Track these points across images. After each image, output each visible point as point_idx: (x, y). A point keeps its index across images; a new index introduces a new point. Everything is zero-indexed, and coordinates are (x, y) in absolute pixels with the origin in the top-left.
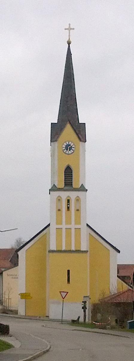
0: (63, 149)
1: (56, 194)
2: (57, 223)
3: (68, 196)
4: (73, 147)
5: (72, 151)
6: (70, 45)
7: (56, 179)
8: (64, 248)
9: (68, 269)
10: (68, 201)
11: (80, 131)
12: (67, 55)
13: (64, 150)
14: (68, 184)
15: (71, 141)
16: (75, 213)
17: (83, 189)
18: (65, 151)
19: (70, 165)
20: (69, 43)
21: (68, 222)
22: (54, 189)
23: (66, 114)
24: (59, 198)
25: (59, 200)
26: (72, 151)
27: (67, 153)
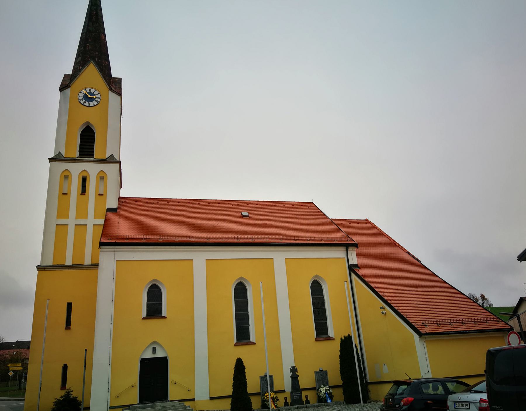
0: (80, 98)
1: (63, 166)
2: (59, 216)
3: (84, 170)
5: (96, 103)
7: (68, 144)
8: (69, 262)
9: (69, 301)
10: (84, 180)
11: (486, 299)
13: (82, 100)
14: (86, 153)
15: (93, 88)
16: (78, 199)
17: (113, 160)
18: (82, 102)
19: (91, 122)
21: (82, 213)
22: (56, 159)
24: (102, 174)
25: (102, 178)
26: (96, 103)
27: (82, 102)
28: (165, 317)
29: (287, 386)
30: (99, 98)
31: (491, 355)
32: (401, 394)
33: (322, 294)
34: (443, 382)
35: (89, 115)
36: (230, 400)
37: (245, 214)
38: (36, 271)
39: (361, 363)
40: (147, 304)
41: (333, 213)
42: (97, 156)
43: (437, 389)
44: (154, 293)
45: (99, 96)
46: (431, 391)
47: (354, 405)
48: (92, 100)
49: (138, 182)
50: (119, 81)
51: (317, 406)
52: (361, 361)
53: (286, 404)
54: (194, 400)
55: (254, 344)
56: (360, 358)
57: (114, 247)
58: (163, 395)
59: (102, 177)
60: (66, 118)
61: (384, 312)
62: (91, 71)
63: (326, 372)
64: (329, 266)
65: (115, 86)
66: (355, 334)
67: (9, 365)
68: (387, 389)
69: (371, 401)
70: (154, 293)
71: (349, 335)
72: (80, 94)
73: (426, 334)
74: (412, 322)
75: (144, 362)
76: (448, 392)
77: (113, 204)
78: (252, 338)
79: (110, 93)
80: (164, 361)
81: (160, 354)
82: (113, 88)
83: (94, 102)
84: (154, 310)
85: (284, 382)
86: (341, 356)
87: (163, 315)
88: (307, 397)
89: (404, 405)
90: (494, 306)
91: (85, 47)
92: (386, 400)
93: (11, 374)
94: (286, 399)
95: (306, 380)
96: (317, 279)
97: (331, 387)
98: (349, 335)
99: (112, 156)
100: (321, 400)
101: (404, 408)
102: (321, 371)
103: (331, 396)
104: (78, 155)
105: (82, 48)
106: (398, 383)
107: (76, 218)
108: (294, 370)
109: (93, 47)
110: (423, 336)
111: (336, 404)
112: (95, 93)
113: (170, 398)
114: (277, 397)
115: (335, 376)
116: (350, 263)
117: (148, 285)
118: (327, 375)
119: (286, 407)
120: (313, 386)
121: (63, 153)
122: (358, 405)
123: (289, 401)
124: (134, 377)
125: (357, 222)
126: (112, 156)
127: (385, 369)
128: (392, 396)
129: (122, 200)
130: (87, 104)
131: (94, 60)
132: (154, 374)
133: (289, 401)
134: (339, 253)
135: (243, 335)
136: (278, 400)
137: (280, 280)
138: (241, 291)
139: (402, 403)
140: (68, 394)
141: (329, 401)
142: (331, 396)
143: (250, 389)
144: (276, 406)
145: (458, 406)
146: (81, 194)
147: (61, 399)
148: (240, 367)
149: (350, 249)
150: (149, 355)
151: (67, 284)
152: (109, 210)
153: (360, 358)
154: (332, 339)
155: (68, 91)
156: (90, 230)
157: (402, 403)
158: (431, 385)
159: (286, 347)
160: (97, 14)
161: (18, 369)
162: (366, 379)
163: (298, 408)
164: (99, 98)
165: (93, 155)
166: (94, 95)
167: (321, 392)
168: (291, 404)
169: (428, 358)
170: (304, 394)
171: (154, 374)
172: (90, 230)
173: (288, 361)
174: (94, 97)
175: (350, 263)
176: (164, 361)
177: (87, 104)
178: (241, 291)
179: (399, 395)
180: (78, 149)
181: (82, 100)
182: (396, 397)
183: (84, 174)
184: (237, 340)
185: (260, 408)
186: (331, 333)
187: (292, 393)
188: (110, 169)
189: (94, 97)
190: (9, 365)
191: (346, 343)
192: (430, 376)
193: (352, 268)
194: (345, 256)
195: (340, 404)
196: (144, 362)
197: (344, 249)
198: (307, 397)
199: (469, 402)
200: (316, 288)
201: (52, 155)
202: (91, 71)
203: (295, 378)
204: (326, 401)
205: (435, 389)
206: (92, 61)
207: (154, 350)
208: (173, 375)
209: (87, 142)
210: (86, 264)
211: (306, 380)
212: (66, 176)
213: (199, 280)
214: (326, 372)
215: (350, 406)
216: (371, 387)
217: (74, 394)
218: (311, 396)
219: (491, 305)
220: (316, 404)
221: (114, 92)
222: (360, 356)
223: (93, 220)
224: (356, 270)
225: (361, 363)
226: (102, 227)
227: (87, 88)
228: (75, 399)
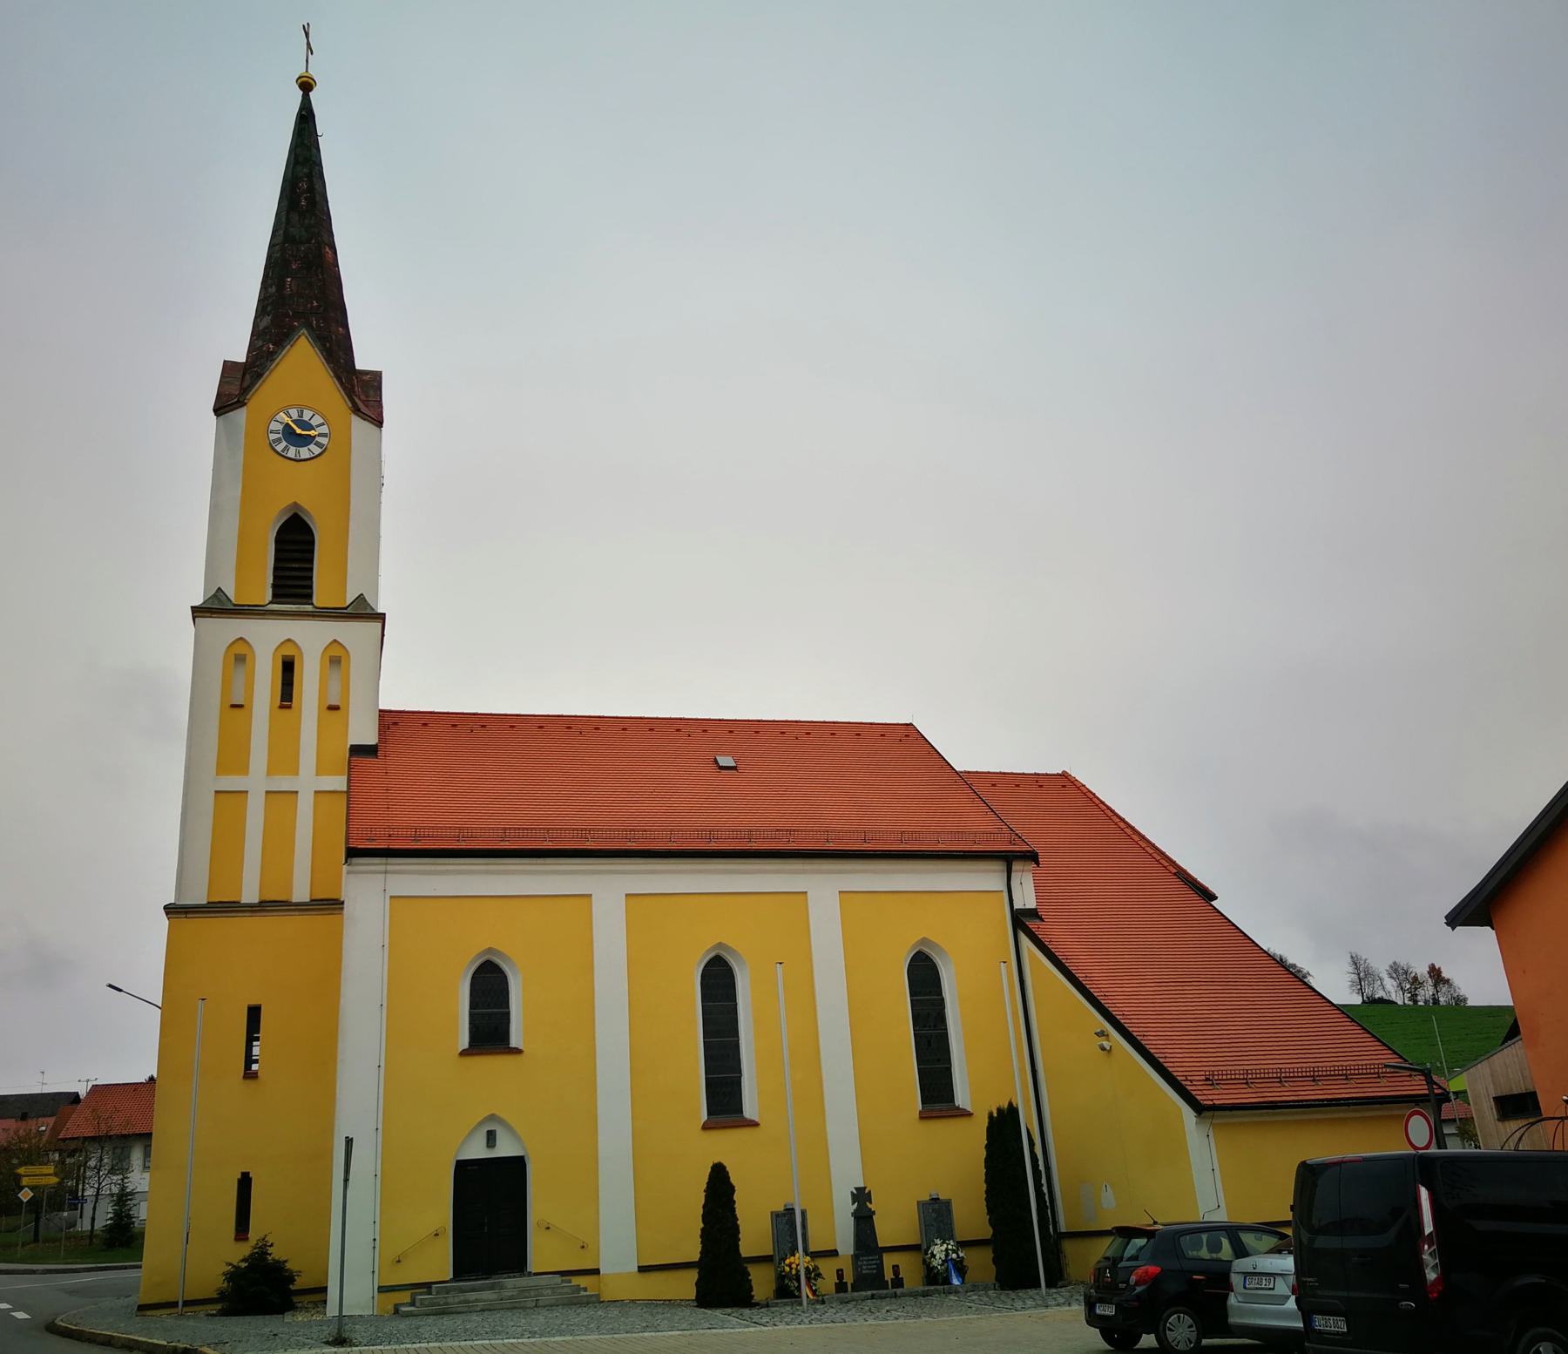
0: (273, 437)
2: (223, 768)
4: (295, 417)
5: (317, 451)
6: (314, 95)
8: (250, 895)
9: (254, 1002)
10: (288, 667)
11: (1447, 981)
12: (301, 109)
13: (278, 441)
15: (310, 409)
17: (363, 612)
19: (305, 503)
20: (306, 86)
21: (284, 758)
22: (213, 608)
23: (321, 1324)
24: (336, 652)
26: (317, 451)
27: (279, 448)
28: (518, 1051)
29: (843, 1236)
30: (324, 435)
31: (1308, 1175)
32: (1133, 1258)
33: (939, 991)
34: (1233, 1232)
35: (294, 484)
36: (693, 1275)
37: (725, 761)
38: (164, 921)
39: (1044, 1181)
40: (471, 1015)
41: (965, 752)
42: (320, 598)
43: (1218, 1248)
44: (489, 986)
45: (324, 429)
46: (1204, 1253)
47: (1021, 1293)
48: (305, 441)
49: (423, 668)
50: (373, 382)
51: (925, 1294)
52: (1044, 1174)
53: (841, 1287)
54: (596, 1272)
55: (754, 1124)
56: (1042, 1168)
57: (383, 860)
58: (515, 1261)
59: (336, 659)
60: (235, 491)
61: (1106, 1044)
62: (302, 357)
63: (948, 1203)
64: (962, 911)
65: (363, 394)
66: (1026, 1101)
67: (21, 1171)
68: (1103, 1248)
69: (1070, 1283)
70: (489, 986)
71: (1010, 1104)
72: (275, 426)
73: (1214, 1108)
74: (1179, 1075)
75: (464, 1169)
76: (1241, 1251)
77: (366, 734)
78: (750, 1110)
79: (356, 421)
80: (516, 1166)
81: (506, 1148)
82: (361, 406)
83: (312, 447)
84: (490, 1031)
85: (835, 1229)
86: (989, 1161)
87: (513, 1044)
88: (896, 1269)
89: (1137, 1283)
90: (1469, 1003)
91: (281, 286)
92: (1099, 1272)
93: (25, 1195)
94: (840, 1273)
95: (896, 1225)
96: (926, 950)
97: (963, 1244)
98: (1010, 1104)
99: (361, 598)
100: (935, 1279)
101: (1139, 1289)
102: (935, 1200)
103: (960, 1268)
104: (269, 597)
105: (273, 290)
106: (1127, 1233)
107: (269, 773)
108: (861, 1196)
109: (302, 286)
110: (1206, 1114)
111: (974, 1289)
112: (314, 422)
113: (532, 1266)
114: (816, 1268)
115: (971, 1216)
116: (1016, 906)
117: (473, 962)
118: (949, 1212)
119: (841, 1295)
120: (913, 1239)
121: (230, 592)
122: (1031, 1292)
123: (849, 1278)
124: (441, 1213)
125: (1038, 780)
126: (361, 598)
127: (1108, 1199)
128: (1113, 1262)
129: (389, 720)
130: (292, 452)
131: (309, 326)
132: (490, 1207)
133: (849, 1278)
134: (988, 879)
135: (724, 1100)
136: (819, 1275)
137: (824, 948)
138: (718, 980)
139: (1133, 1279)
140: (261, 1253)
141: (956, 1282)
142: (960, 1268)
143: (747, 1248)
144: (814, 1292)
145: (1252, 1283)
146: (281, 707)
147: (244, 1265)
148: (719, 1186)
149: (1016, 866)
150: (477, 1150)
151: (250, 959)
152: (357, 750)
153: (1042, 1168)
154: (966, 1114)
155: (240, 416)
156: (305, 807)
157: (1133, 1279)
158: (1204, 1237)
159: (841, 1134)
160: (311, 189)
161: (44, 1181)
162: (1055, 1223)
163: (873, 1297)
164: (324, 435)
165: (310, 596)
166: (312, 428)
167: (933, 1256)
168: (854, 1289)
169: (1217, 1172)
170: (889, 1261)
171: (490, 1207)
172: (305, 807)
173: (846, 1173)
174: (312, 433)
175: (1016, 906)
176: (516, 1166)
177: (292, 452)
178: (718, 980)
179: (1129, 1259)
180: (270, 580)
181: (278, 441)
182: (1123, 1264)
183: (288, 652)
184: (710, 1113)
185: (772, 1295)
186: (962, 1098)
187: (856, 1257)
188: (352, 633)
189: (312, 433)
190: (21, 1171)
191: (1004, 1125)
192: (1221, 1216)
193: (1021, 920)
194: (1003, 887)
195: (986, 1288)
196: (464, 1169)
197: (1000, 866)
198: (896, 1269)
199: (1273, 1275)
200: (924, 975)
201: (199, 602)
202: (302, 357)
203: (864, 1219)
204: (947, 1281)
205: (1216, 1247)
206: (304, 331)
207: (491, 1138)
208: (542, 1202)
209: (295, 561)
210: (295, 899)
211: (896, 1225)
212: (240, 656)
213: (608, 948)
214: (948, 1203)
215: (1012, 1294)
216: (1068, 1247)
217: (276, 1253)
218: (909, 1267)
219: (1460, 1001)
220: (921, 1288)
221: (365, 417)
222: (1041, 1163)
223: (316, 779)
224: (1032, 924)
225: (1044, 1181)
226: (342, 803)
227: (292, 407)
228: (279, 1267)
